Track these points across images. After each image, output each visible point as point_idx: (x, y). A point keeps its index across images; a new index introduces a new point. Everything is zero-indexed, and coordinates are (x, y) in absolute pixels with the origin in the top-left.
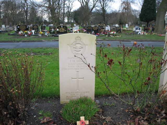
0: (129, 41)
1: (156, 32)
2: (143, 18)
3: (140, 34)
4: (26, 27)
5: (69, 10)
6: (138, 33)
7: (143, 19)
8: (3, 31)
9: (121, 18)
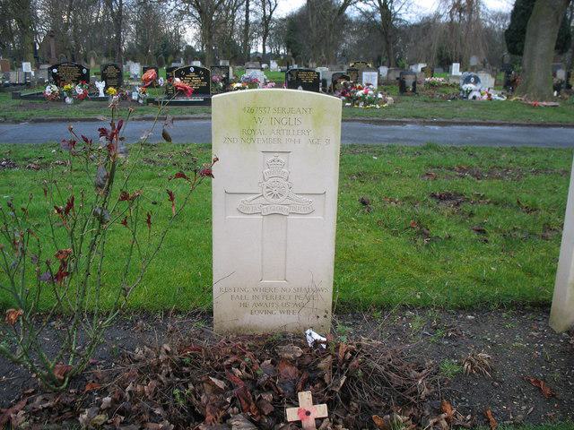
0: (402, 123)
1: (524, 91)
2: (517, 42)
3: (474, 98)
4: (81, 71)
5: (268, 13)
6: (471, 97)
7: (518, 45)
8: (15, 85)
9: (444, 43)
